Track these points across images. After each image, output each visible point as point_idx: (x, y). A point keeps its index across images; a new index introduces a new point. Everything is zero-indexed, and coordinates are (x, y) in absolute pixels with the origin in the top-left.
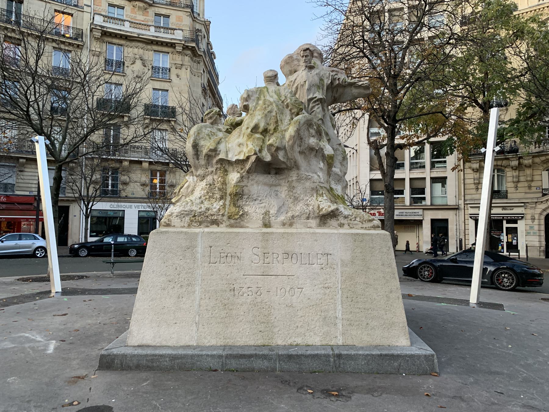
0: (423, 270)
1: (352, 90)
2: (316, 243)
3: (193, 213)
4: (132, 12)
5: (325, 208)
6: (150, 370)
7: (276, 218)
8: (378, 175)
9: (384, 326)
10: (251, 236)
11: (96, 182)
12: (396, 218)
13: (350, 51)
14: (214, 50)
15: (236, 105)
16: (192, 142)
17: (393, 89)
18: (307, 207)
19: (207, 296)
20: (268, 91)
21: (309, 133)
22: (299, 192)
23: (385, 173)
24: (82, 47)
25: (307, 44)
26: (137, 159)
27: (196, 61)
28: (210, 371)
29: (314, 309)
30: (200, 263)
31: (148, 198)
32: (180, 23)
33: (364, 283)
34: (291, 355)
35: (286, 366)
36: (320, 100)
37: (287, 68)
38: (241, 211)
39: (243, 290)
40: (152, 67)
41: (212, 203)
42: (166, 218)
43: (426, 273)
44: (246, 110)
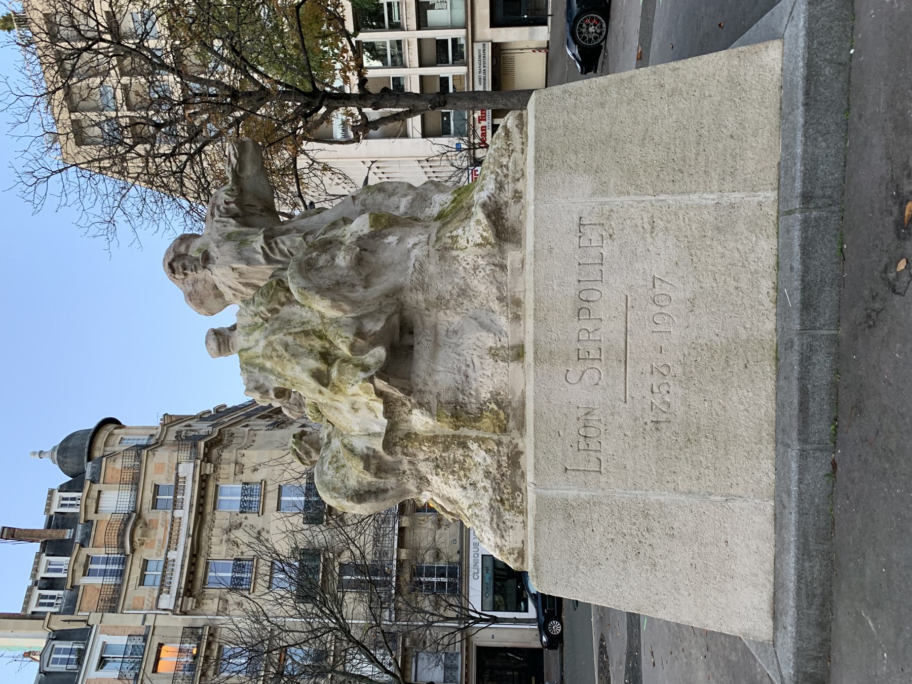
0: (586, 35)
1: (248, 177)
2: (556, 251)
3: (496, 504)
4: (152, 547)
6: (831, 602)
7: (503, 333)
8: (414, 123)
9: (737, 100)
11: (437, 606)
12: (489, 88)
14: (211, 407)
18: (480, 269)
19: (669, 479)
20: (246, 350)
21: (326, 266)
22: (450, 287)
23: (410, 111)
24: (212, 629)
26: (396, 537)
27: (229, 439)
28: (835, 477)
29: (698, 252)
30: (600, 491)
32: (166, 468)
33: (643, 145)
34: (802, 304)
35: (827, 314)
36: (268, 239)
37: (211, 302)
38: (491, 406)
39: (657, 402)
40: (241, 512)
41: (475, 465)
42: (507, 559)
43: (591, 29)
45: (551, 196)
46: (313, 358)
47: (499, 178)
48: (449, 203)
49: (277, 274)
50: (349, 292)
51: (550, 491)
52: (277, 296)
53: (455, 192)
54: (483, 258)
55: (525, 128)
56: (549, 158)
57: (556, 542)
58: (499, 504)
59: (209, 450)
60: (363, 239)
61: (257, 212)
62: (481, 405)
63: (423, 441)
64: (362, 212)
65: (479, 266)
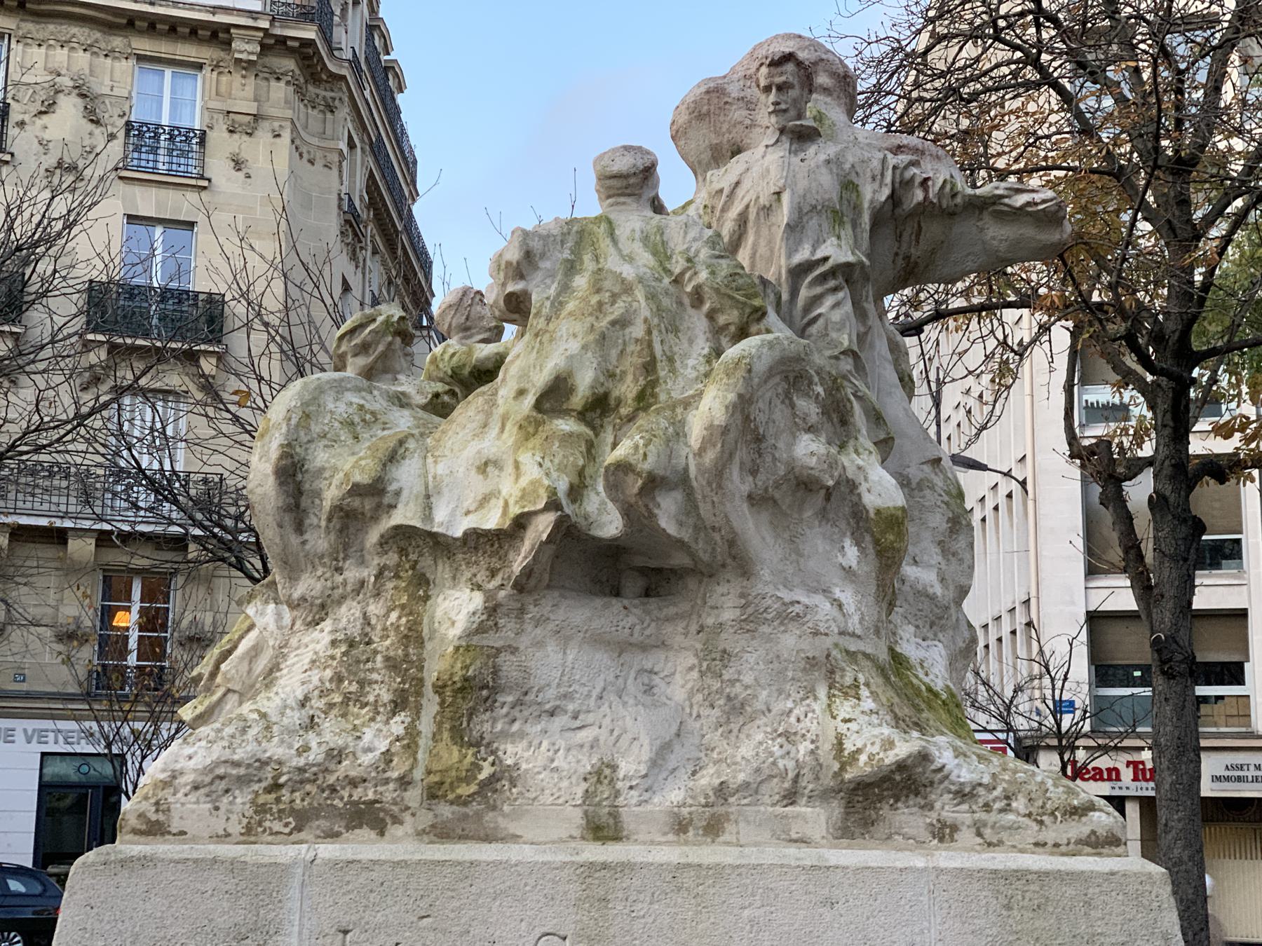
1: (982, 230)
2: (828, 915)
3: (268, 773)
5: (869, 749)
7: (646, 796)
10: (531, 882)
13: (977, 60)
14: (401, 53)
15: (479, 293)
16: (274, 453)
17: (1175, 222)
18: (787, 747)
21: (794, 415)
22: (748, 679)
23: (1150, 588)
25: (789, 37)
26: (43, 522)
31: (87, 697)
36: (846, 273)
37: (702, 138)
40: (128, 123)
41: (355, 728)
42: (146, 798)
44: (516, 316)
45: (946, 905)
46: (596, 380)
47: (981, 791)
48: (926, 680)
49: (769, 291)
50: (742, 463)
51: (298, 895)
52: (731, 307)
53: (952, 695)
54: (812, 752)
55: (1089, 850)
56: (1026, 903)
57: (185, 906)
58: (270, 781)
59: (292, 51)
60: (851, 492)
61: (904, 246)
62: (489, 744)
63: (411, 614)
64: (904, 482)
65: (794, 743)
